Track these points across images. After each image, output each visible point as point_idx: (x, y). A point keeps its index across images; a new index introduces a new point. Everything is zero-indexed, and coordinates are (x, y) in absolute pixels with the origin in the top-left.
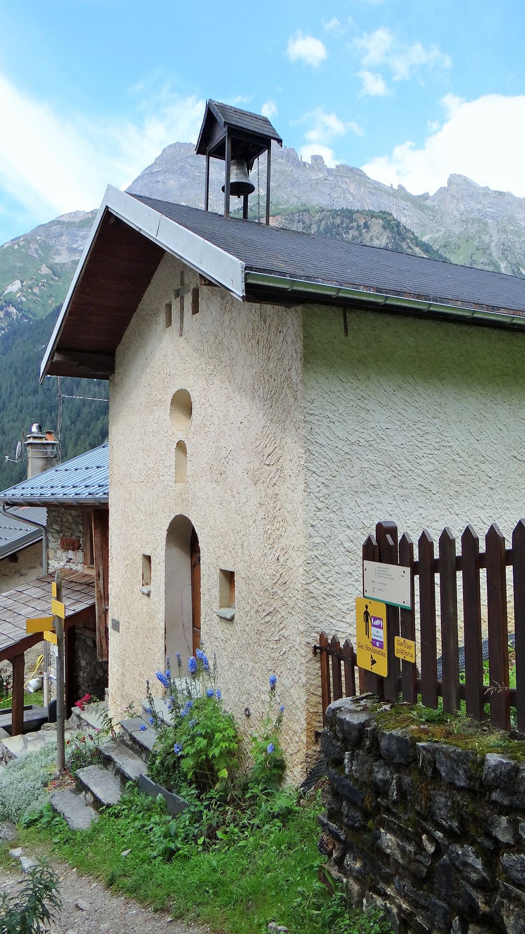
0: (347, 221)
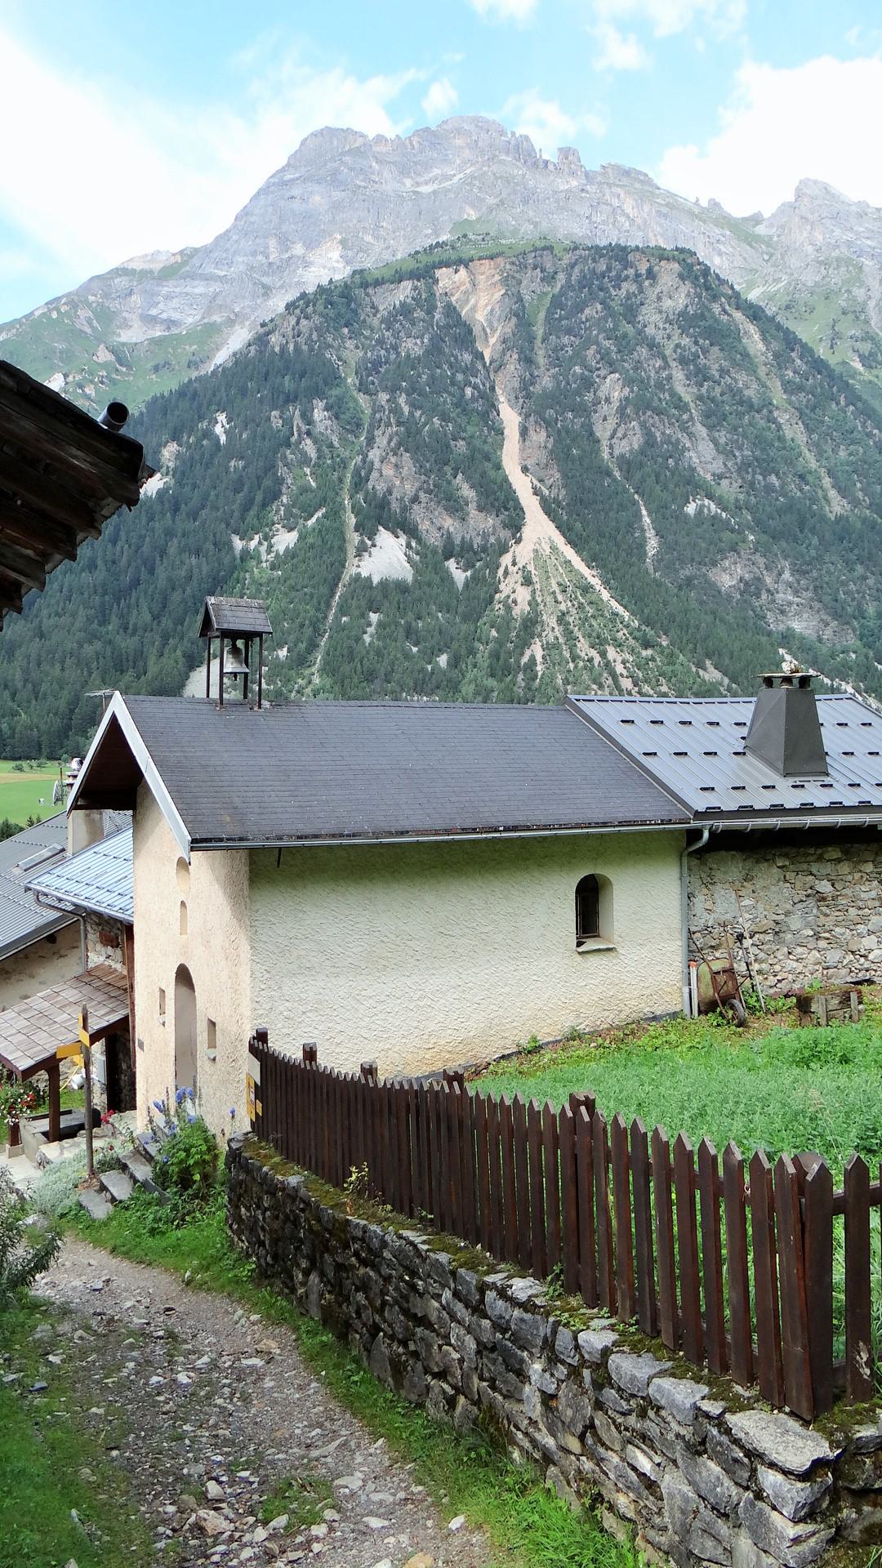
0: (617, 265)
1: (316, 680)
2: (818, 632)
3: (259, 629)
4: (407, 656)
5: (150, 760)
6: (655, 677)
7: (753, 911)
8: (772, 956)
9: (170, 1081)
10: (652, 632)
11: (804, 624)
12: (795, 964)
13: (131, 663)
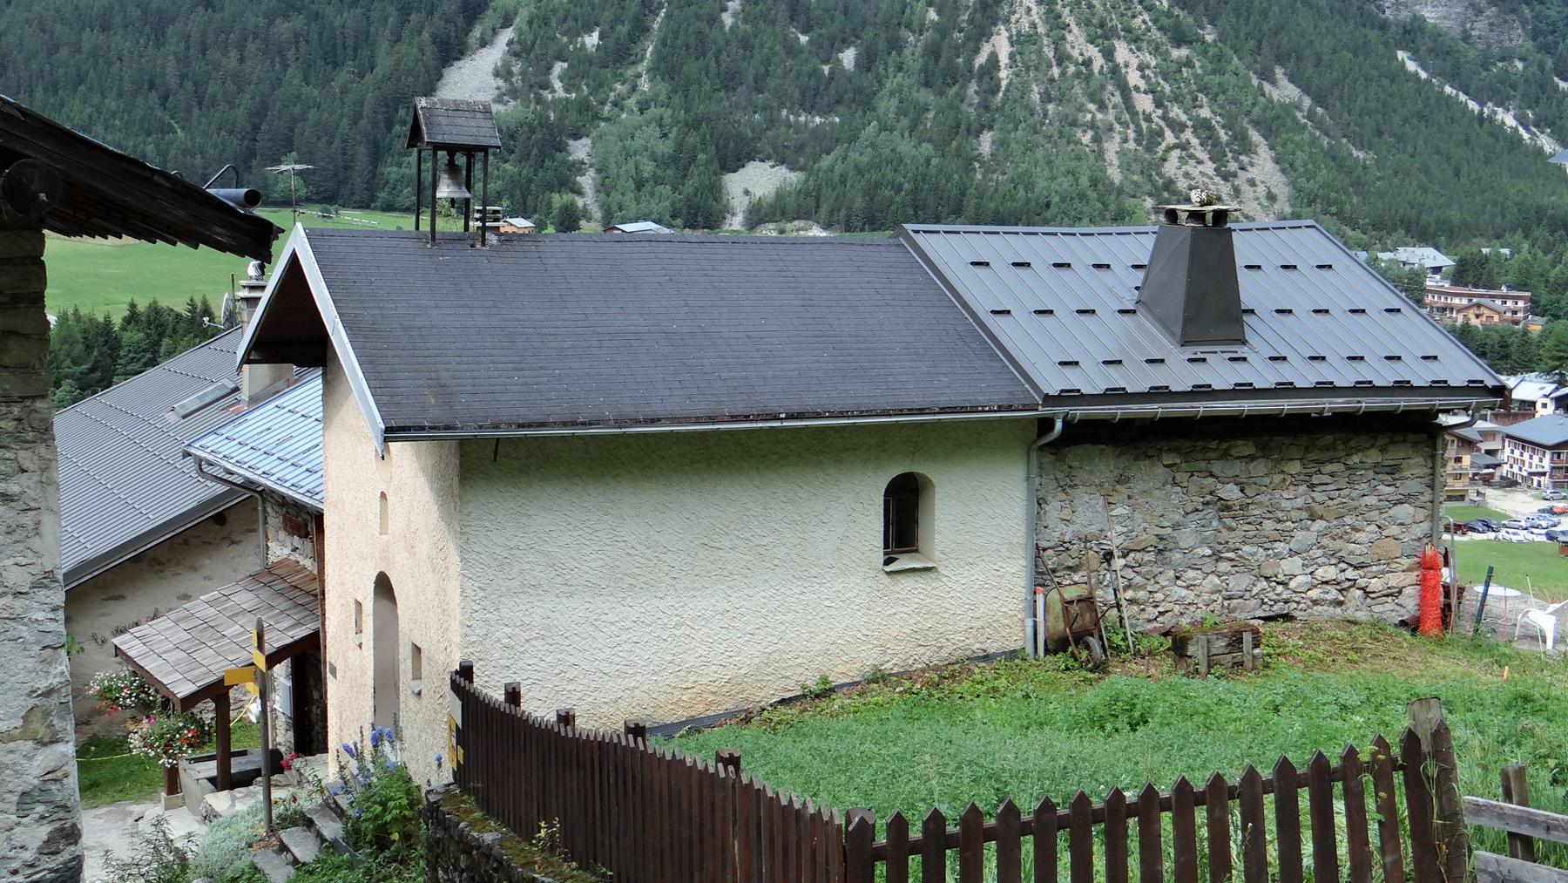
1: (645, 85)
2: (1463, 24)
3: (484, 142)
4: (792, 49)
5: (338, 320)
6: (1191, 92)
7: (1128, 522)
8: (1152, 581)
9: (368, 716)
10: (1190, 20)
11: (1442, 11)
12: (1184, 592)
13: (350, 52)
